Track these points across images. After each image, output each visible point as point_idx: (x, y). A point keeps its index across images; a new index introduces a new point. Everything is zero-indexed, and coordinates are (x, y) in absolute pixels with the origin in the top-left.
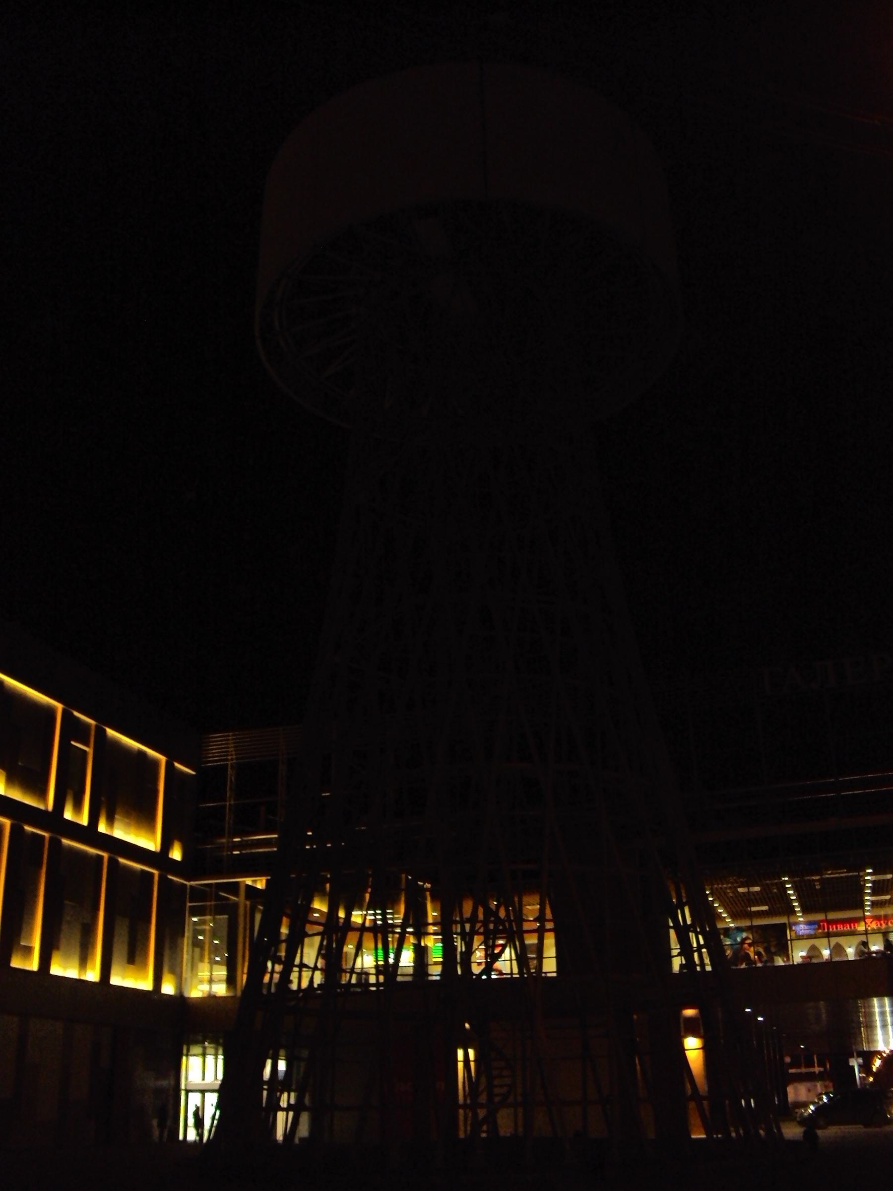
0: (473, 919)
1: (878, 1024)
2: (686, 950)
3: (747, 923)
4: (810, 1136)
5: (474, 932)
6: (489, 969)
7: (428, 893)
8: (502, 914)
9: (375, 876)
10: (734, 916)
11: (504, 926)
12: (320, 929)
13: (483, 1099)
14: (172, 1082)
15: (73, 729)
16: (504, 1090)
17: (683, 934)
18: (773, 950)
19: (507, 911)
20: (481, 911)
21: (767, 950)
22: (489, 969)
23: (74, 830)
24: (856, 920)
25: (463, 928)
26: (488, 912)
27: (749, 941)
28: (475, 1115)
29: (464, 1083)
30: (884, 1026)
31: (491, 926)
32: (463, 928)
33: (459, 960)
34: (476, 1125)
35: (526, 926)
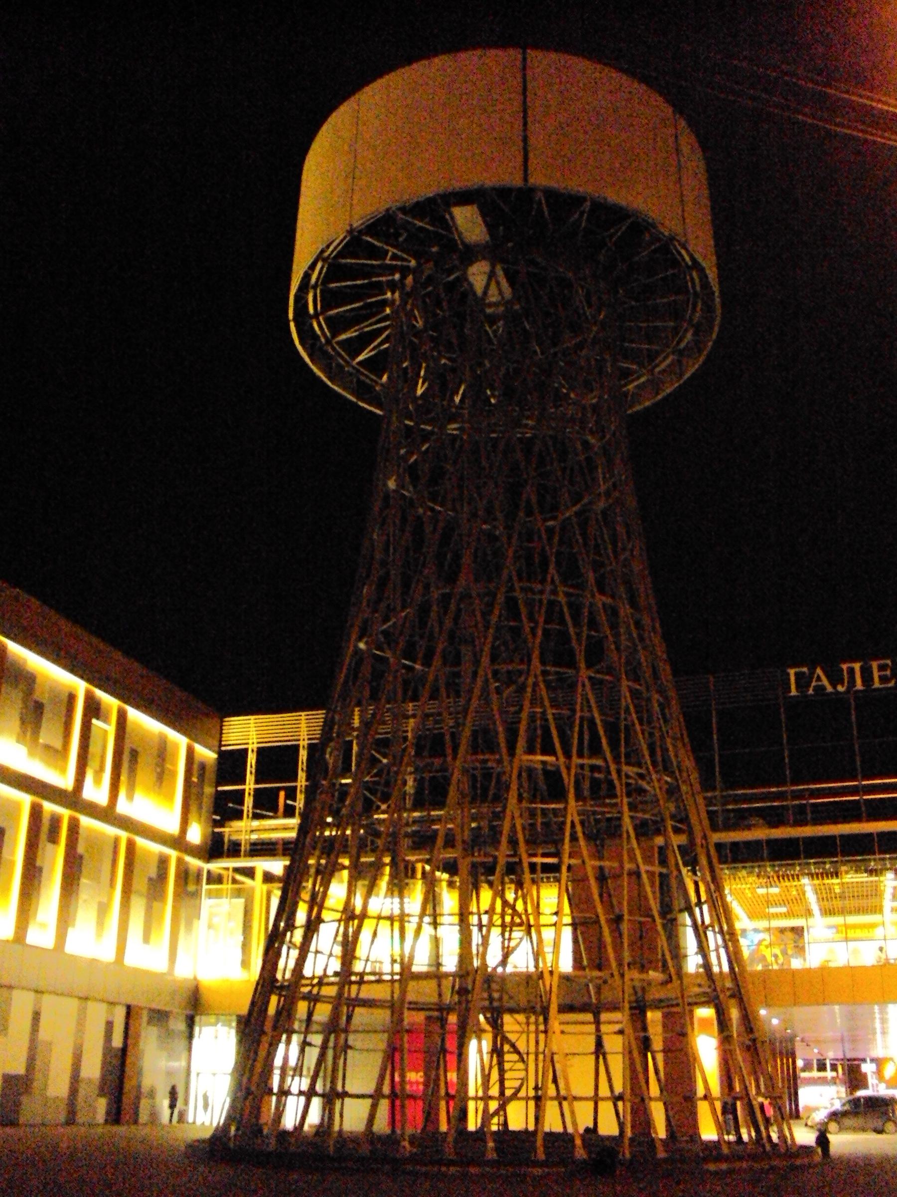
0: (490, 912)
1: (878, 1031)
2: (702, 949)
3: (764, 924)
4: (823, 1140)
5: (491, 924)
6: (504, 963)
7: (425, 813)
8: (520, 906)
9: (387, 854)
10: (752, 916)
11: (520, 917)
12: (338, 916)
13: (494, 1091)
14: (184, 1063)
15: (93, 709)
16: (517, 1084)
17: (700, 932)
18: (790, 952)
19: (525, 903)
20: (499, 902)
21: (784, 952)
22: (504, 963)
23: (92, 810)
24: (872, 926)
25: (480, 920)
26: (505, 903)
27: (765, 943)
28: (486, 1107)
29: (647, 1082)
30: (884, 1033)
31: (508, 919)
32: (480, 920)
33: (354, 400)
34: (487, 1117)
35: (543, 920)
